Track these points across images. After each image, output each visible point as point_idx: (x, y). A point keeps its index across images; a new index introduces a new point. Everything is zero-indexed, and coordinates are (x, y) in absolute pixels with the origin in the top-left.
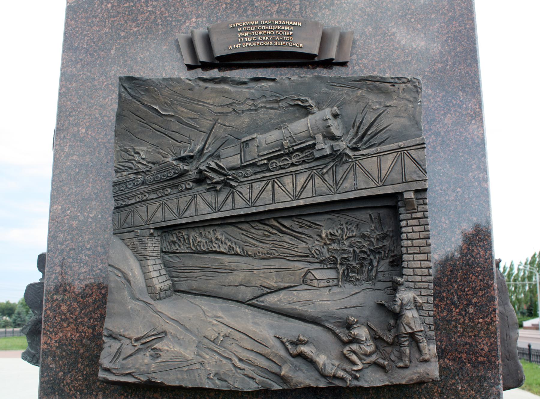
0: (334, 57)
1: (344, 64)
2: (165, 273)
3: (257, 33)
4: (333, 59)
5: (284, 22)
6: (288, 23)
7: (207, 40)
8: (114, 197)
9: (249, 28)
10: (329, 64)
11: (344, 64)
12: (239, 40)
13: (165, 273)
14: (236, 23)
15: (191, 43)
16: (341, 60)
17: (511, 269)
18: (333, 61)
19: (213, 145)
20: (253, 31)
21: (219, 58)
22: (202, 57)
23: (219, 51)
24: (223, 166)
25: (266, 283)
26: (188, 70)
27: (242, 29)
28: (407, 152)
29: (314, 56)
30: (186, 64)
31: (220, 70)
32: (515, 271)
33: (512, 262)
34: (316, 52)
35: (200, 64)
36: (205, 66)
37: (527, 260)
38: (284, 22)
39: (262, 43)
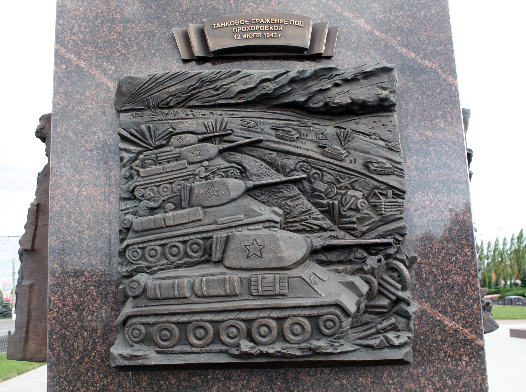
1: (329, 58)
3: (276, 28)
4: (322, 54)
5: (218, 24)
6: (224, 24)
7: (202, 35)
11: (329, 58)
12: (235, 36)
14: (272, 17)
15: (186, 37)
16: (329, 54)
17: (496, 245)
18: (322, 55)
22: (198, 51)
23: (214, 45)
26: (184, 63)
28: (157, 137)
29: (306, 49)
31: (214, 64)
32: (501, 247)
33: (497, 238)
34: (308, 46)
36: (200, 60)
37: (513, 236)
38: (218, 24)
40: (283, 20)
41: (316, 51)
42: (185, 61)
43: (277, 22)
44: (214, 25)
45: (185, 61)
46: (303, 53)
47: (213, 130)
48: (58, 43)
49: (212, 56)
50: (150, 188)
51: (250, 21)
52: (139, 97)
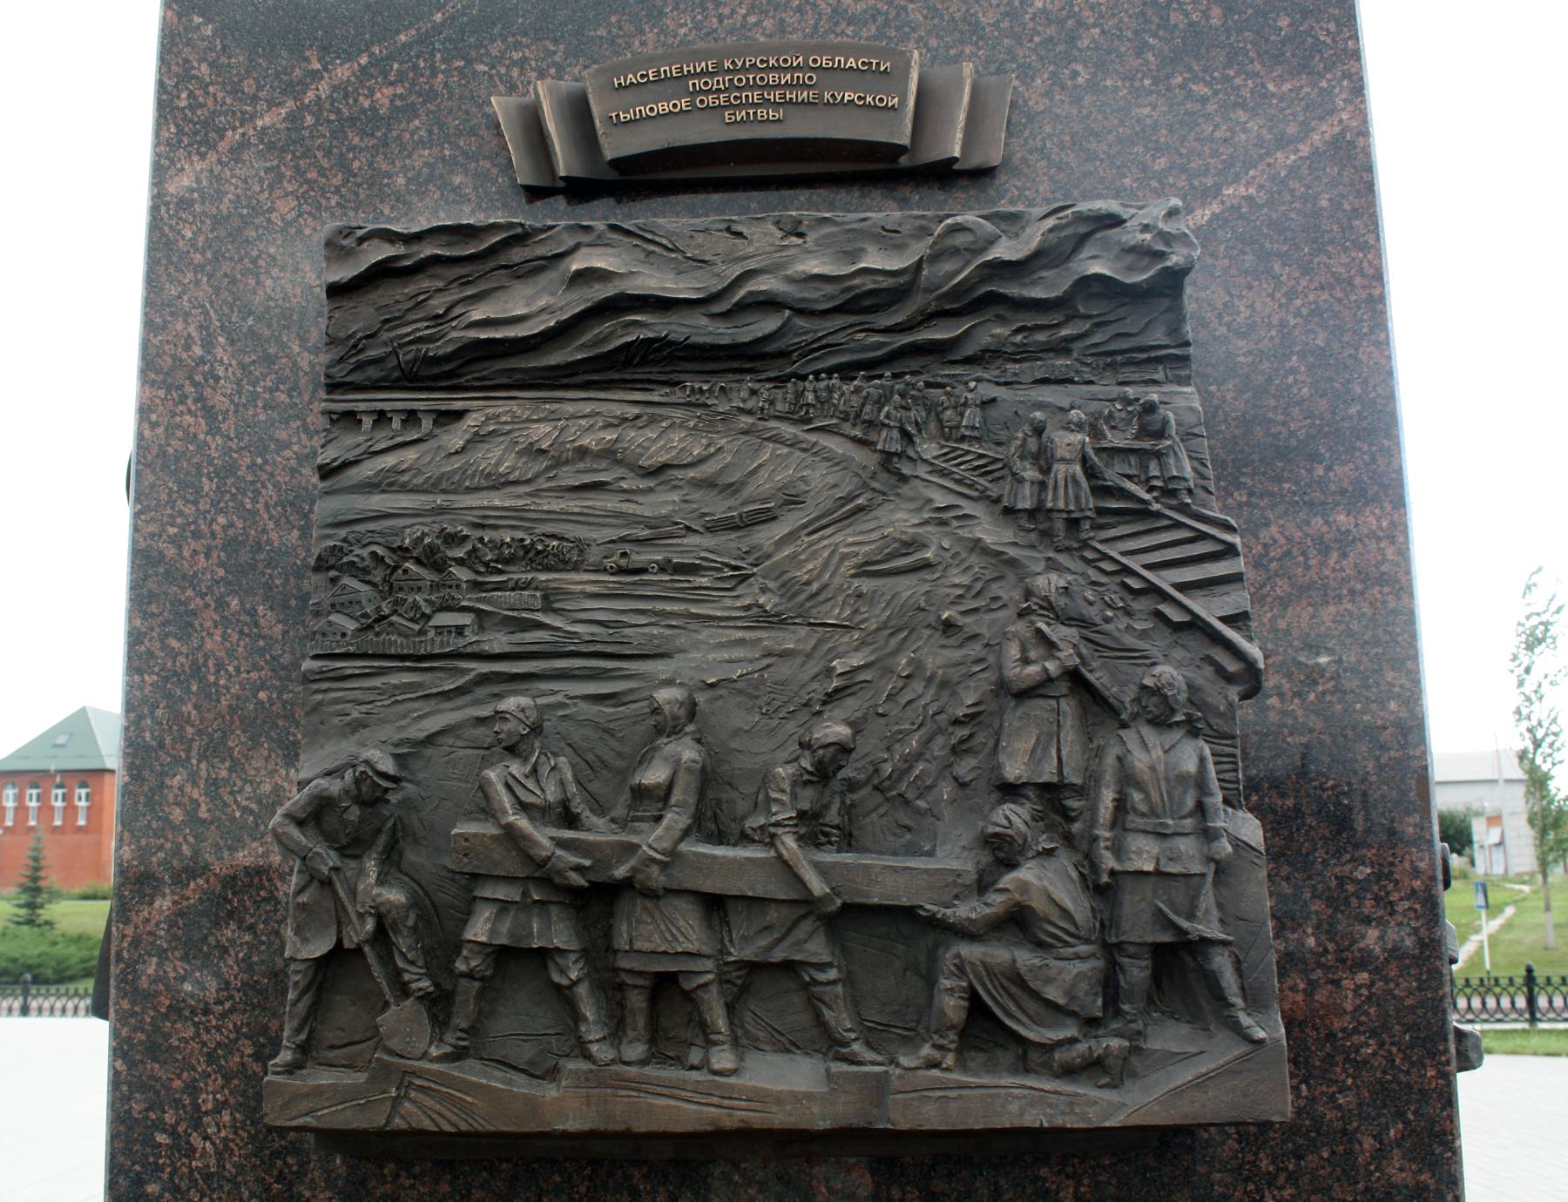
0: (957, 154)
2: (590, 1046)
3: (740, 80)
4: (956, 160)
5: (630, 76)
6: (692, 69)
7: (579, 111)
8: (333, 387)
9: (706, 83)
10: (944, 175)
11: (982, 175)
13: (590, 1046)
16: (975, 161)
18: (956, 167)
19: (550, 223)
20: (719, 90)
21: (616, 163)
22: (565, 163)
23: (614, 146)
24: (583, 307)
25: (667, 502)
26: (530, 201)
27: (692, 103)
29: (901, 150)
30: (523, 186)
34: (905, 140)
35: (562, 184)
39: (735, 98)
40: (703, 64)
41: (934, 154)
42: (534, 193)
43: (689, 71)
44: (874, 62)
45: (534, 193)
46: (895, 160)
47: (1232, 763)
48: (1389, 450)
49: (612, 175)
50: (367, 470)
51: (719, 65)
52: (544, 378)
